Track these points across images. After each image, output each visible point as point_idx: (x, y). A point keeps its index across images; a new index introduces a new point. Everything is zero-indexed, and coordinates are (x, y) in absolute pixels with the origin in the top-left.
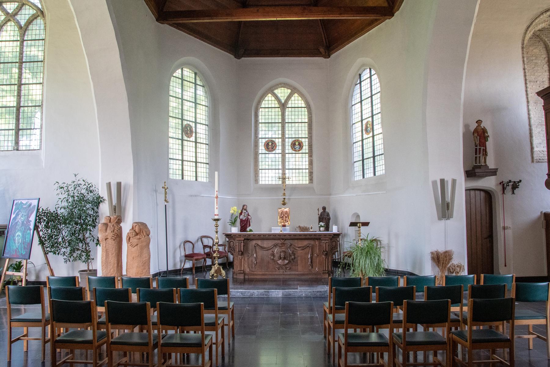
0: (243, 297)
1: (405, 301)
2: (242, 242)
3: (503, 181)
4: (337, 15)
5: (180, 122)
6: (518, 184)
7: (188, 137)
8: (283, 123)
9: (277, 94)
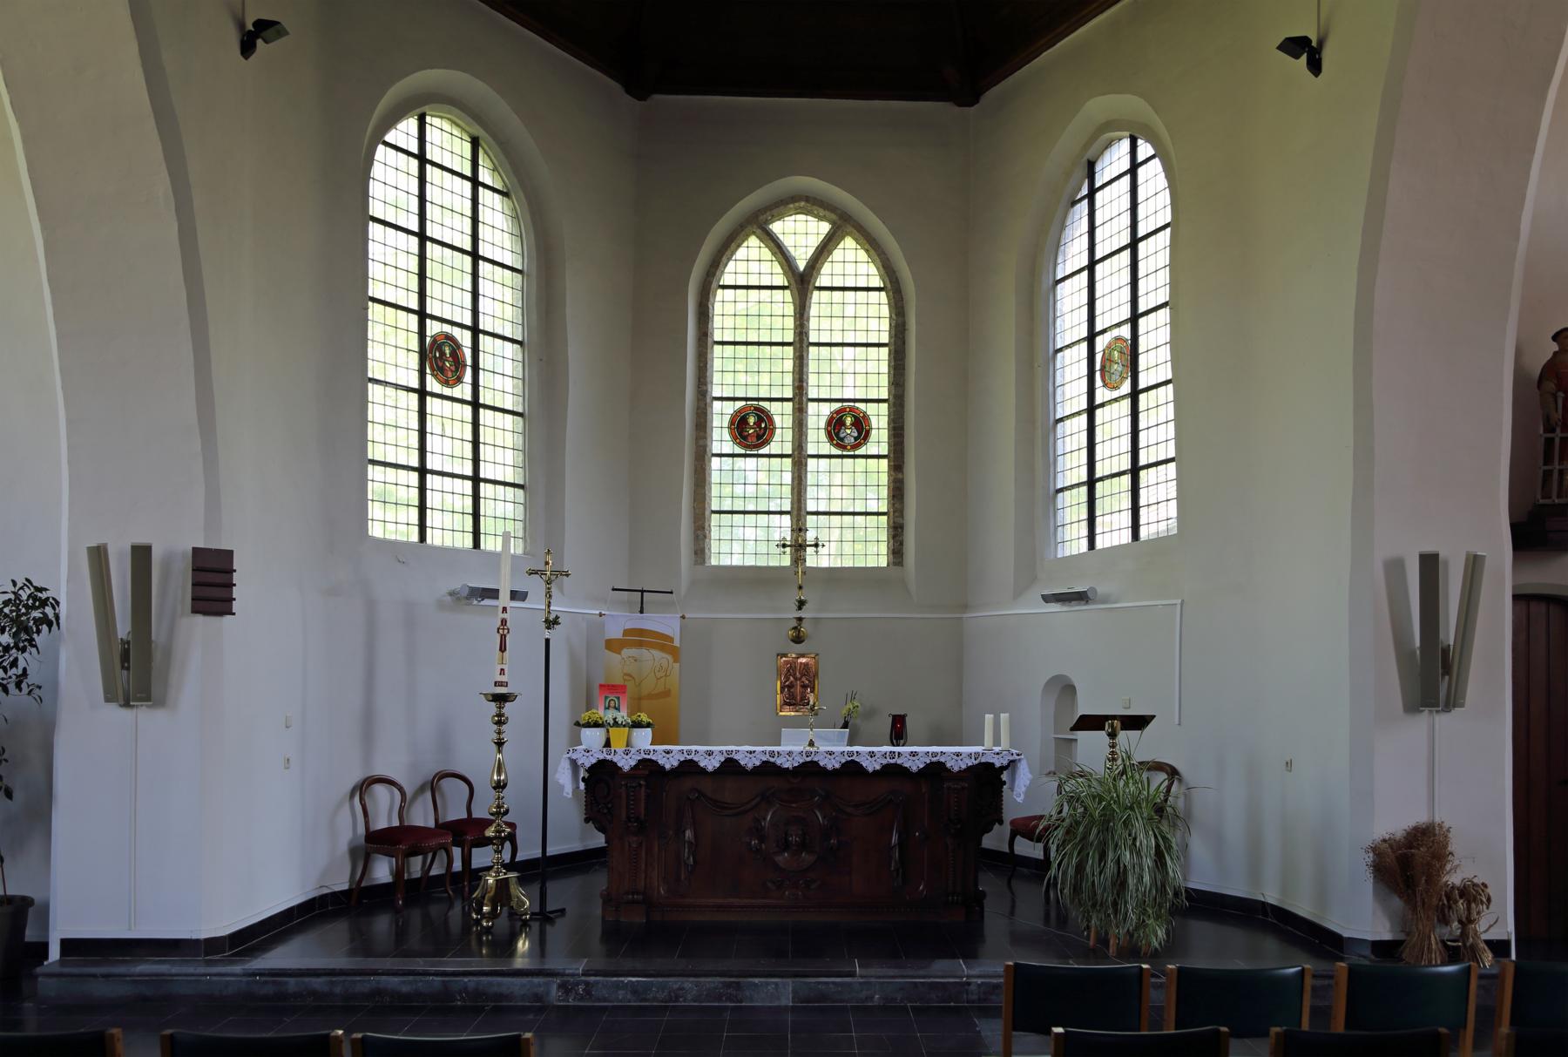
1: (1278, 1029)
2: (642, 782)
5: (414, 325)
7: (446, 383)
8: (801, 343)
9: (781, 237)
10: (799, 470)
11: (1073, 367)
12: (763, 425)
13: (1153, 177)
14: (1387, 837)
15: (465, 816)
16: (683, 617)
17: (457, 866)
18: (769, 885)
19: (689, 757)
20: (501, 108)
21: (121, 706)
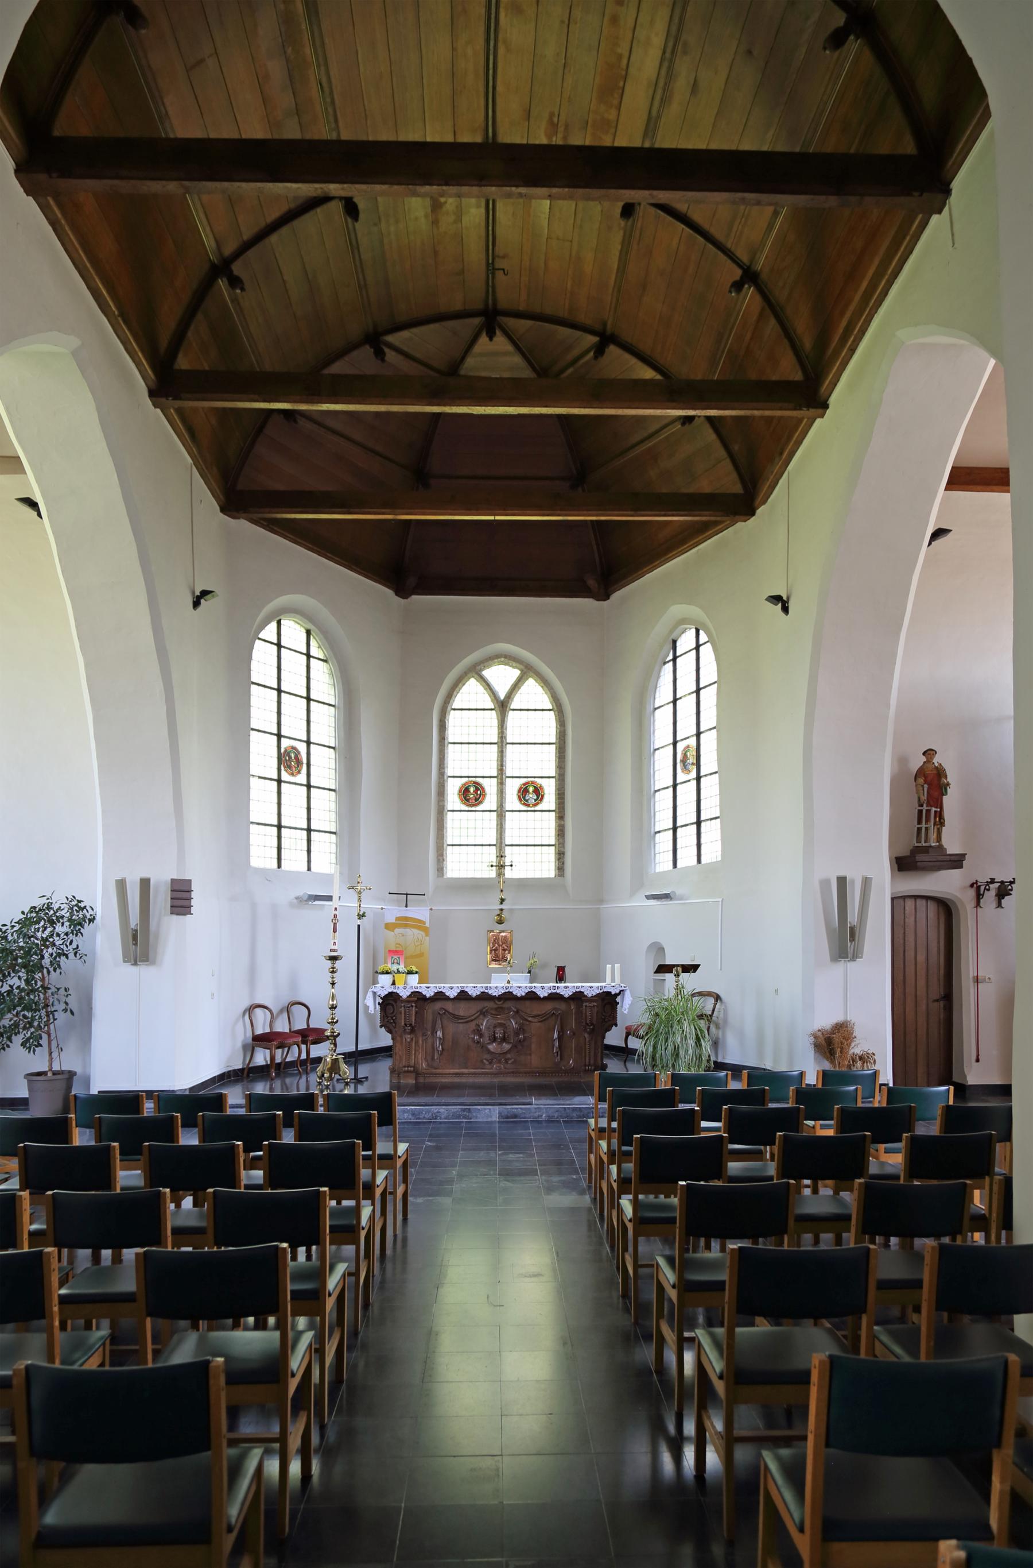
0: (417, 1122)
2: (413, 1005)
3: (977, 881)
4: (629, 513)
6: (1010, 887)
8: (502, 743)
10: (501, 819)
11: (663, 762)
12: (479, 792)
13: (707, 652)
14: (820, 1028)
15: (306, 1027)
16: (431, 909)
17: (304, 1056)
18: (484, 1061)
19: (440, 990)
20: (324, 613)
21: (132, 965)
